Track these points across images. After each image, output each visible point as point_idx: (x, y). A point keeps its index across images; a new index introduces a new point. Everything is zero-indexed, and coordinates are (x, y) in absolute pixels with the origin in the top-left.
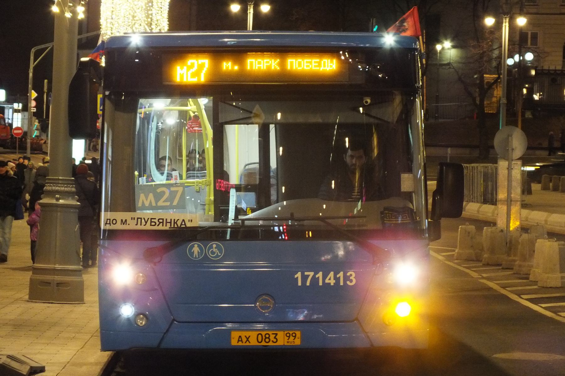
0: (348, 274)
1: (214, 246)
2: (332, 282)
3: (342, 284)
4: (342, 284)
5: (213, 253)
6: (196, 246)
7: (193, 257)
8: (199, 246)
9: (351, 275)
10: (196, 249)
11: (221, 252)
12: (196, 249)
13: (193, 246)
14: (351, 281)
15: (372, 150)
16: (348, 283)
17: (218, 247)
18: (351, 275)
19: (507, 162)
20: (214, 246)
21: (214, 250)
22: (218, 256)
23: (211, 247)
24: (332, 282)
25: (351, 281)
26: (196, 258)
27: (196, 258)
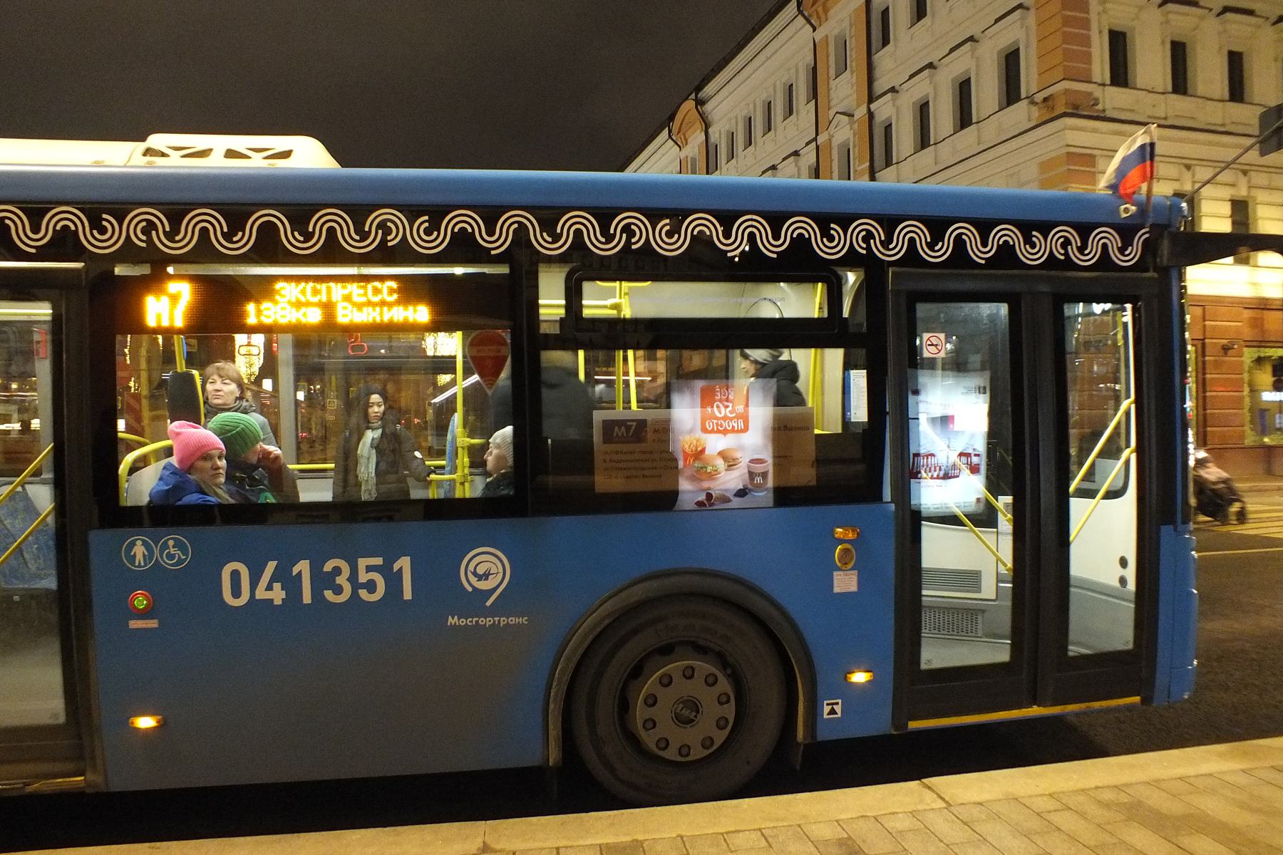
0: (328, 567)
1: (171, 543)
2: (278, 595)
3: (307, 598)
4: (307, 598)
5: (171, 557)
6: (139, 543)
7: (133, 563)
8: (144, 543)
9: (337, 571)
10: (139, 550)
11: (185, 552)
12: (139, 550)
13: (133, 544)
14: (338, 590)
15: (377, 447)
16: (329, 594)
17: (178, 544)
18: (337, 571)
19: (587, 313)
20: (171, 543)
21: (172, 551)
22: (180, 562)
23: (165, 546)
24: (278, 595)
25: (338, 590)
26: (139, 566)
27: (139, 566)
